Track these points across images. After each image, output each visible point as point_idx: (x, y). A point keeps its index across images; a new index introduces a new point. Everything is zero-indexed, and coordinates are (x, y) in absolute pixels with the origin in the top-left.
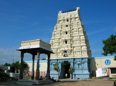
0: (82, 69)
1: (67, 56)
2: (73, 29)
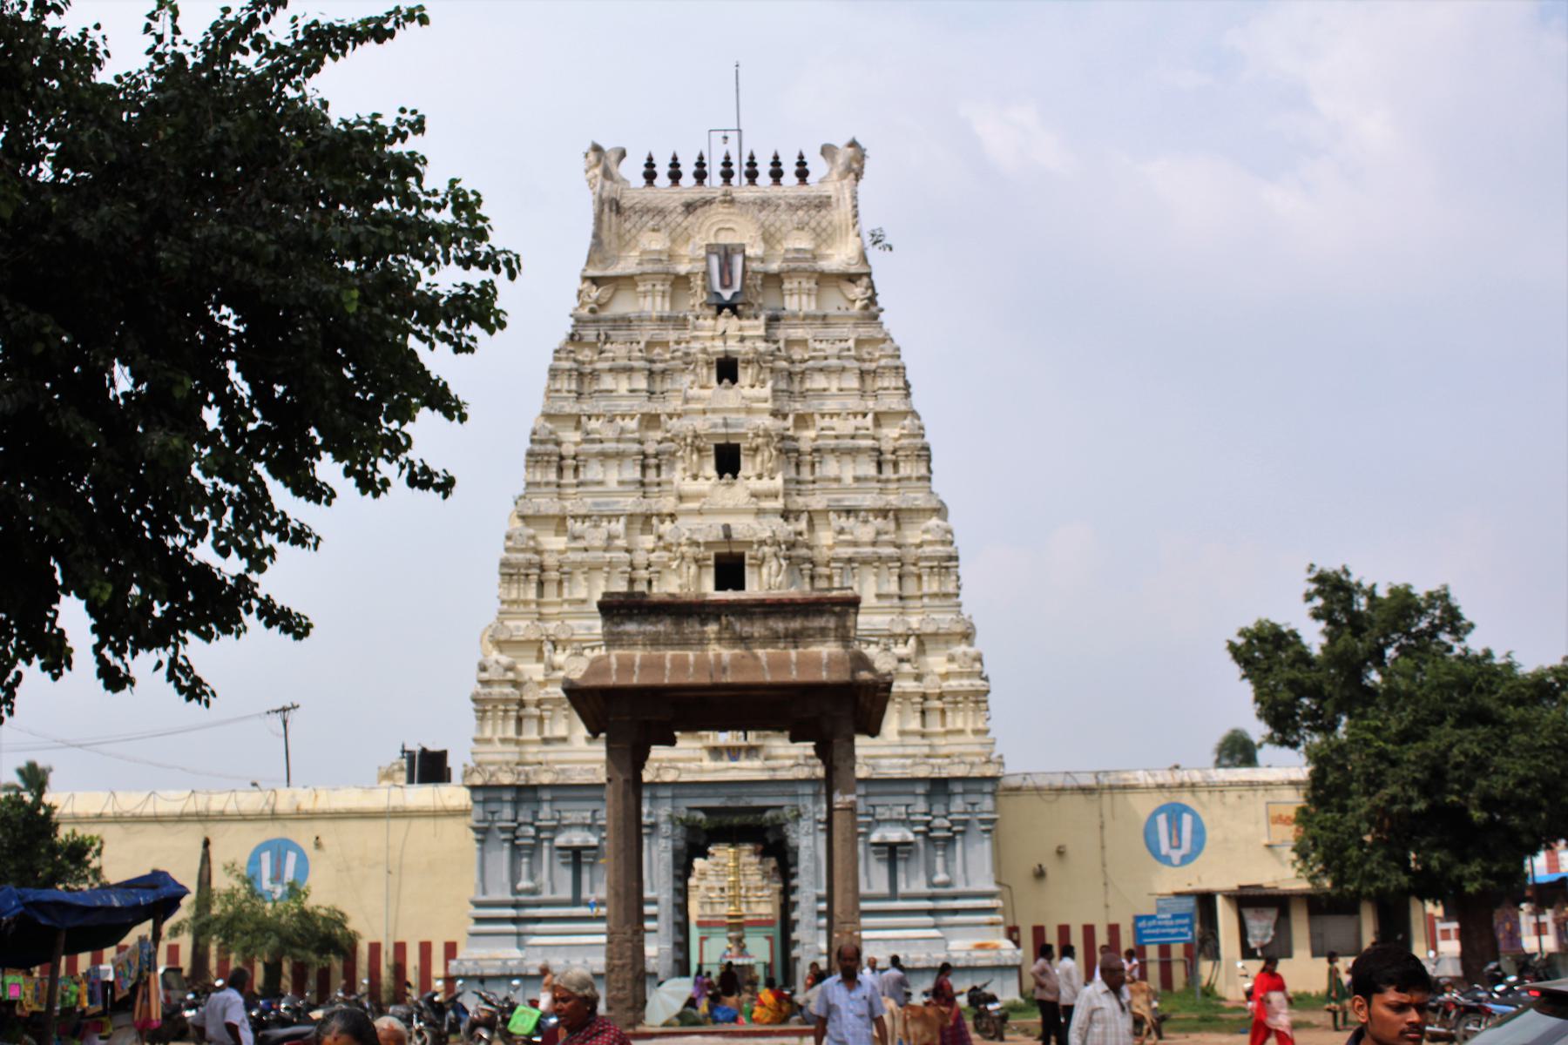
2: (802, 420)
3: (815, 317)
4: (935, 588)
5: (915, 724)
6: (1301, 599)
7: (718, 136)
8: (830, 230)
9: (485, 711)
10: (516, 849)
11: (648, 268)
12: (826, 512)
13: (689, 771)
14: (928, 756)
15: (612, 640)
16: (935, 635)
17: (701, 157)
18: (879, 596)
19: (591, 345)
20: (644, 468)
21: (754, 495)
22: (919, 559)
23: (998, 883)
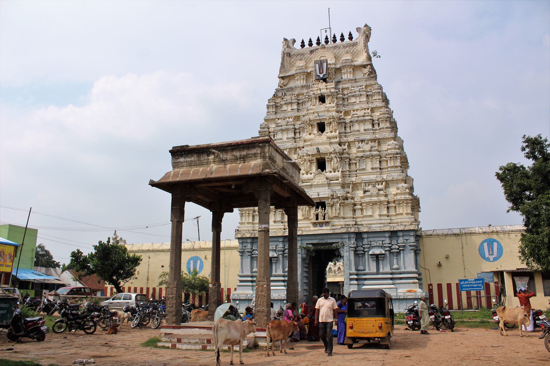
0: (392, 279)
1: (327, 223)
2: (347, 113)
3: (352, 80)
4: (392, 164)
5: (385, 212)
6: (520, 150)
7: (323, 31)
8: (357, 52)
9: (242, 214)
10: (252, 258)
11: (298, 71)
12: (354, 142)
13: (306, 231)
14: (390, 223)
15: (175, 165)
16: (392, 180)
17: (318, 38)
18: (372, 169)
19: (280, 97)
20: (295, 133)
21: (329, 138)
22: (386, 155)
23: (416, 269)
